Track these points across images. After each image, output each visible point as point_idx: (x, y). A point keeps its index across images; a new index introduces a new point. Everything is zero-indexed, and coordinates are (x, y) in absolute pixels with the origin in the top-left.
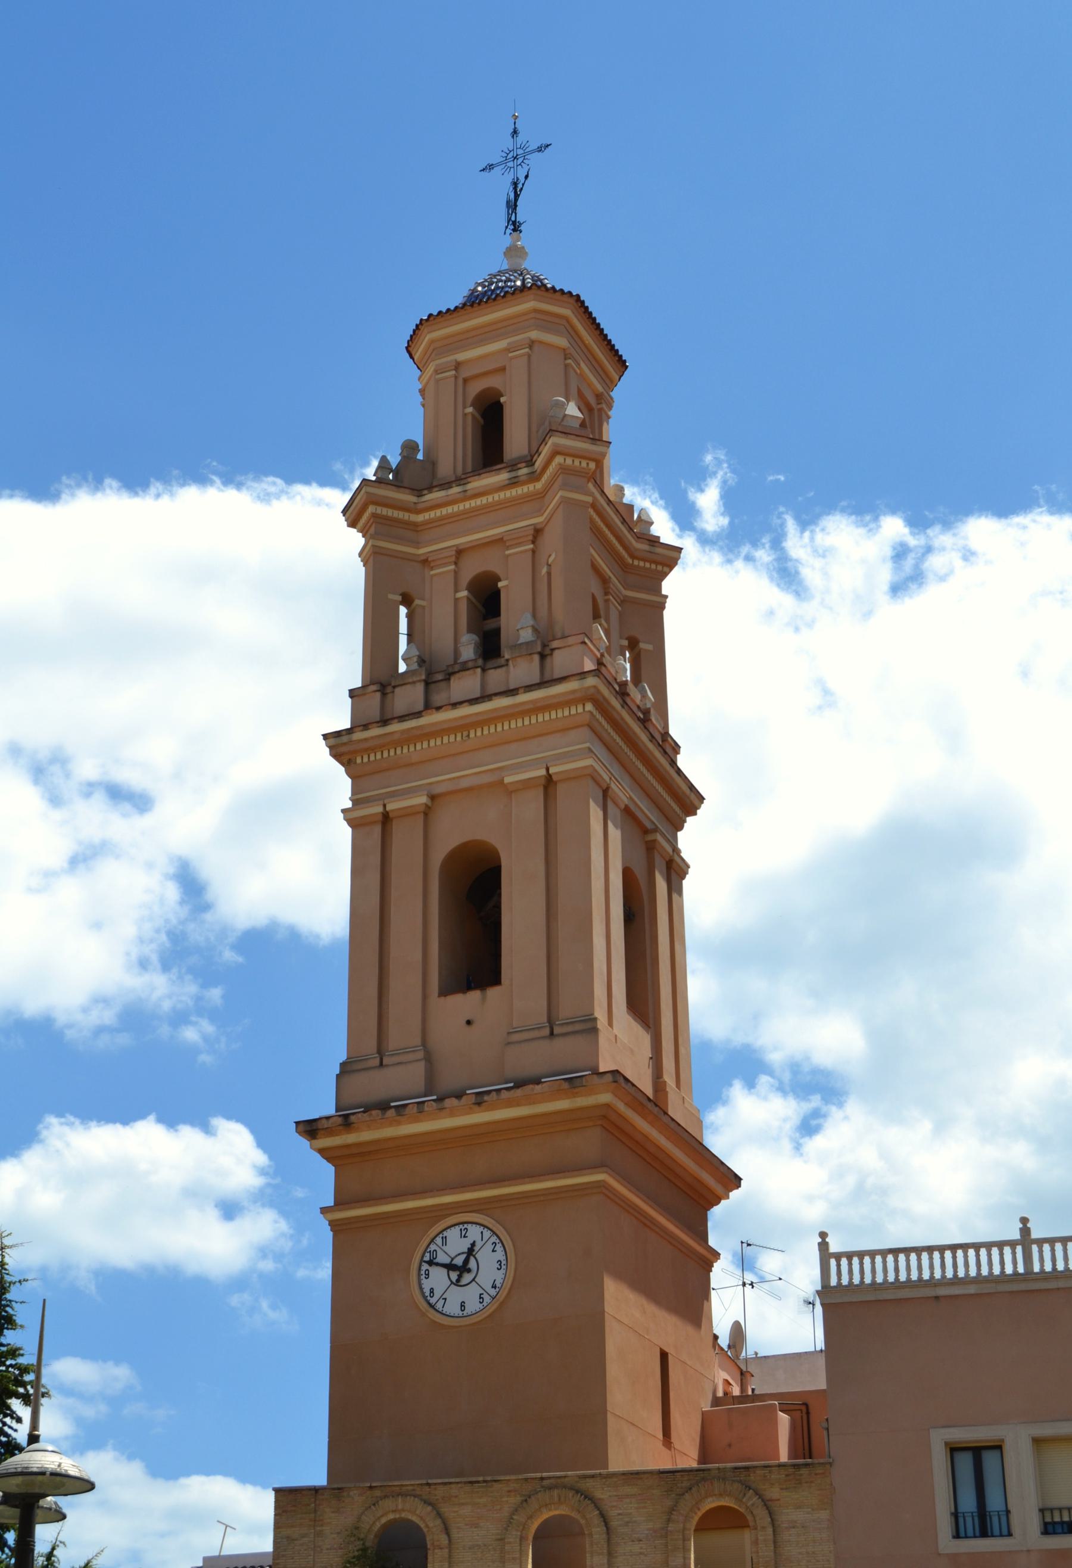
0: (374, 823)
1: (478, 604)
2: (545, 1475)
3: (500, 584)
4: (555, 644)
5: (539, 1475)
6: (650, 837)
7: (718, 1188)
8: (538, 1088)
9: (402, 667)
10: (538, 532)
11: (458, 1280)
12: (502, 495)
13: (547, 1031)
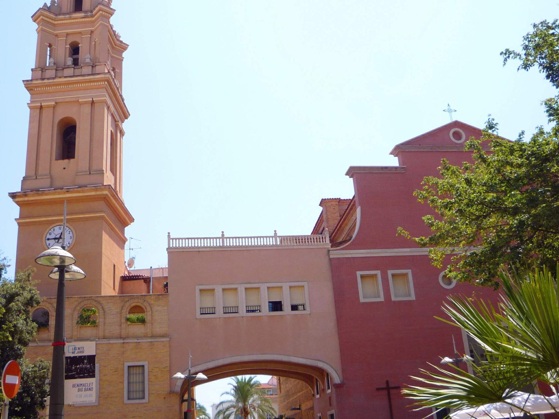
2: (86, 296)
3: (79, 45)
5: (84, 296)
6: (117, 123)
7: (129, 221)
8: (86, 188)
11: (58, 242)
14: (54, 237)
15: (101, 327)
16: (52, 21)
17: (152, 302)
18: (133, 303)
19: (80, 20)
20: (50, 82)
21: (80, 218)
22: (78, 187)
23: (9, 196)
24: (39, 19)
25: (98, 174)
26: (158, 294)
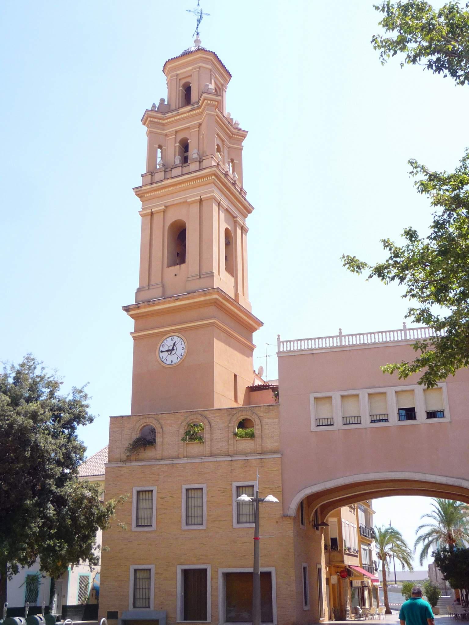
0: (149, 215)
1: (181, 147)
2: (192, 410)
4: (204, 158)
5: (190, 410)
7: (256, 326)
8: (195, 294)
9: (158, 167)
10: (200, 125)
11: (170, 354)
13: (199, 277)
14: (167, 350)
15: (208, 444)
16: (160, 121)
17: (261, 414)
18: (241, 416)
20: (158, 186)
21: (191, 327)
23: (123, 309)
24: (147, 122)
25: (207, 277)
26: (268, 404)
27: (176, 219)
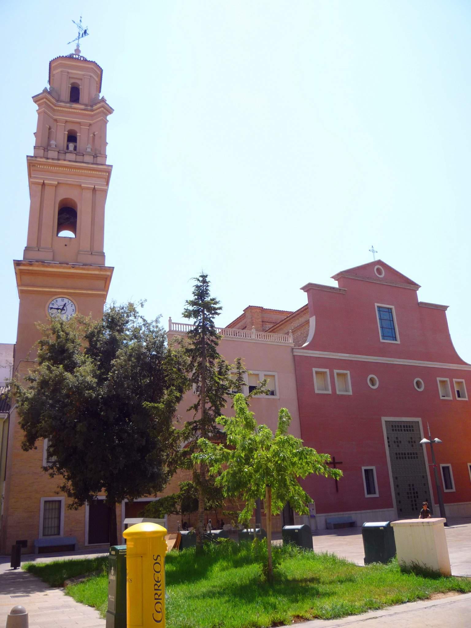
12: (81, 111)
13: (90, 253)
19: (79, 111)
22: (83, 265)
25: (99, 255)
27: (67, 197)
